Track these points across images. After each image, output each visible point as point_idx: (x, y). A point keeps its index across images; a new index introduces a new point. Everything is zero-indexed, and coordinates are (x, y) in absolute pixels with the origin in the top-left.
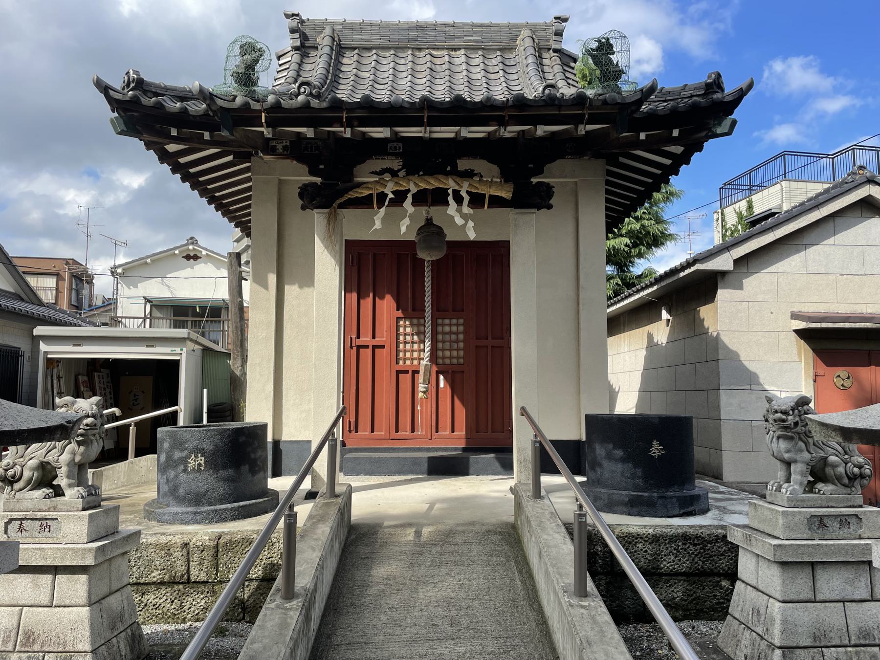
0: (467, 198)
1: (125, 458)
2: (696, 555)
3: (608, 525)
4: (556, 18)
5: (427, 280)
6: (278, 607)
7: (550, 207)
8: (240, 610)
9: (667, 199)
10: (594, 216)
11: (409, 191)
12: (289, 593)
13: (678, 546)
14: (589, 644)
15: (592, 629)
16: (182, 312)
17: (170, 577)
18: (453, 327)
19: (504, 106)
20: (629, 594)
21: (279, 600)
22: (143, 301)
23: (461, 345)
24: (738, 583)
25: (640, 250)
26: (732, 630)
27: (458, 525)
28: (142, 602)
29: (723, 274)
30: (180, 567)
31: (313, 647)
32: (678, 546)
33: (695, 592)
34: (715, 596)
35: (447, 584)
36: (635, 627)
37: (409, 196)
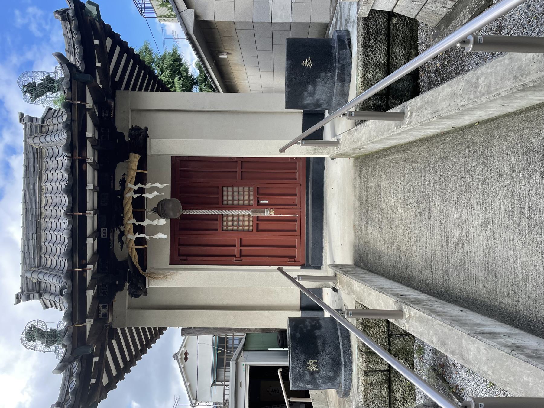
0: (140, 185)
1: (310, 403)
2: (376, 39)
3: (357, 96)
4: (20, 121)
5: (196, 213)
6: (408, 322)
7: (147, 129)
8: (407, 337)
9: (150, 53)
10: (156, 99)
11: (134, 224)
12: (399, 314)
13: (370, 51)
14: (437, 112)
15: (426, 109)
16: (220, 362)
17: (385, 383)
18: (229, 194)
19: (72, 159)
20: (400, 84)
21: (403, 321)
22: (214, 386)
23: (241, 189)
24: (395, 11)
25: (183, 70)
26: (425, 16)
27: (355, 195)
28: (401, 400)
29: (196, 16)
30: (379, 376)
31: (434, 296)
32: (370, 51)
33: (400, 41)
34: (402, 28)
35: (393, 204)
36: (422, 81)
37: (137, 223)
